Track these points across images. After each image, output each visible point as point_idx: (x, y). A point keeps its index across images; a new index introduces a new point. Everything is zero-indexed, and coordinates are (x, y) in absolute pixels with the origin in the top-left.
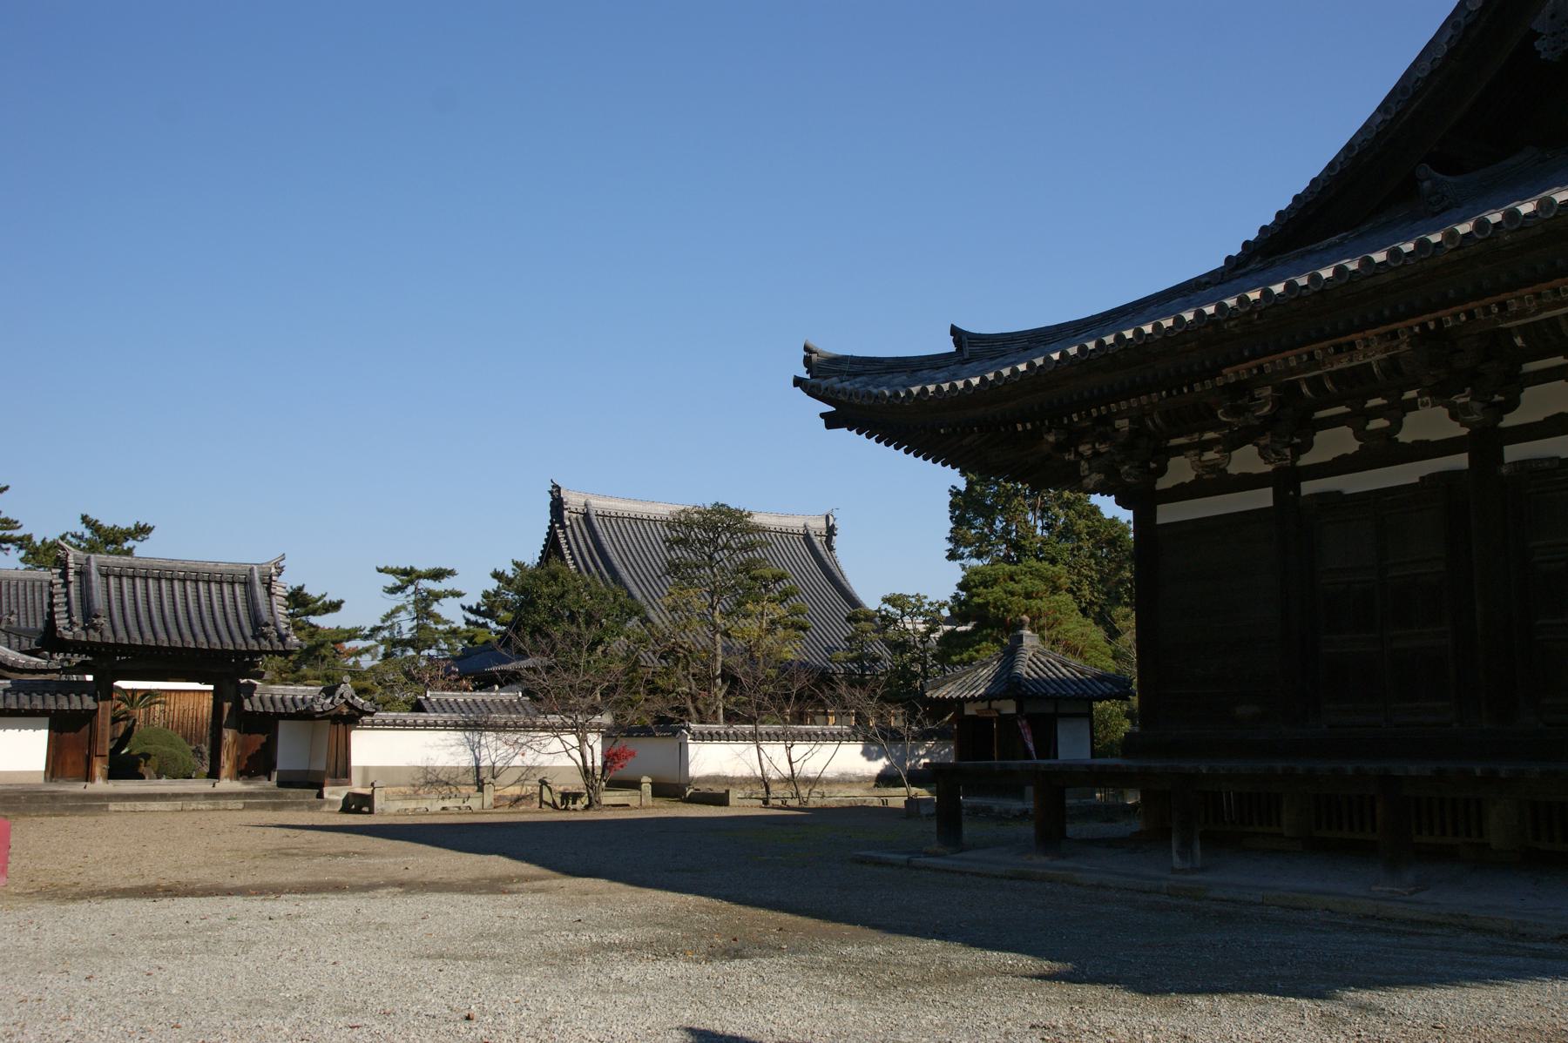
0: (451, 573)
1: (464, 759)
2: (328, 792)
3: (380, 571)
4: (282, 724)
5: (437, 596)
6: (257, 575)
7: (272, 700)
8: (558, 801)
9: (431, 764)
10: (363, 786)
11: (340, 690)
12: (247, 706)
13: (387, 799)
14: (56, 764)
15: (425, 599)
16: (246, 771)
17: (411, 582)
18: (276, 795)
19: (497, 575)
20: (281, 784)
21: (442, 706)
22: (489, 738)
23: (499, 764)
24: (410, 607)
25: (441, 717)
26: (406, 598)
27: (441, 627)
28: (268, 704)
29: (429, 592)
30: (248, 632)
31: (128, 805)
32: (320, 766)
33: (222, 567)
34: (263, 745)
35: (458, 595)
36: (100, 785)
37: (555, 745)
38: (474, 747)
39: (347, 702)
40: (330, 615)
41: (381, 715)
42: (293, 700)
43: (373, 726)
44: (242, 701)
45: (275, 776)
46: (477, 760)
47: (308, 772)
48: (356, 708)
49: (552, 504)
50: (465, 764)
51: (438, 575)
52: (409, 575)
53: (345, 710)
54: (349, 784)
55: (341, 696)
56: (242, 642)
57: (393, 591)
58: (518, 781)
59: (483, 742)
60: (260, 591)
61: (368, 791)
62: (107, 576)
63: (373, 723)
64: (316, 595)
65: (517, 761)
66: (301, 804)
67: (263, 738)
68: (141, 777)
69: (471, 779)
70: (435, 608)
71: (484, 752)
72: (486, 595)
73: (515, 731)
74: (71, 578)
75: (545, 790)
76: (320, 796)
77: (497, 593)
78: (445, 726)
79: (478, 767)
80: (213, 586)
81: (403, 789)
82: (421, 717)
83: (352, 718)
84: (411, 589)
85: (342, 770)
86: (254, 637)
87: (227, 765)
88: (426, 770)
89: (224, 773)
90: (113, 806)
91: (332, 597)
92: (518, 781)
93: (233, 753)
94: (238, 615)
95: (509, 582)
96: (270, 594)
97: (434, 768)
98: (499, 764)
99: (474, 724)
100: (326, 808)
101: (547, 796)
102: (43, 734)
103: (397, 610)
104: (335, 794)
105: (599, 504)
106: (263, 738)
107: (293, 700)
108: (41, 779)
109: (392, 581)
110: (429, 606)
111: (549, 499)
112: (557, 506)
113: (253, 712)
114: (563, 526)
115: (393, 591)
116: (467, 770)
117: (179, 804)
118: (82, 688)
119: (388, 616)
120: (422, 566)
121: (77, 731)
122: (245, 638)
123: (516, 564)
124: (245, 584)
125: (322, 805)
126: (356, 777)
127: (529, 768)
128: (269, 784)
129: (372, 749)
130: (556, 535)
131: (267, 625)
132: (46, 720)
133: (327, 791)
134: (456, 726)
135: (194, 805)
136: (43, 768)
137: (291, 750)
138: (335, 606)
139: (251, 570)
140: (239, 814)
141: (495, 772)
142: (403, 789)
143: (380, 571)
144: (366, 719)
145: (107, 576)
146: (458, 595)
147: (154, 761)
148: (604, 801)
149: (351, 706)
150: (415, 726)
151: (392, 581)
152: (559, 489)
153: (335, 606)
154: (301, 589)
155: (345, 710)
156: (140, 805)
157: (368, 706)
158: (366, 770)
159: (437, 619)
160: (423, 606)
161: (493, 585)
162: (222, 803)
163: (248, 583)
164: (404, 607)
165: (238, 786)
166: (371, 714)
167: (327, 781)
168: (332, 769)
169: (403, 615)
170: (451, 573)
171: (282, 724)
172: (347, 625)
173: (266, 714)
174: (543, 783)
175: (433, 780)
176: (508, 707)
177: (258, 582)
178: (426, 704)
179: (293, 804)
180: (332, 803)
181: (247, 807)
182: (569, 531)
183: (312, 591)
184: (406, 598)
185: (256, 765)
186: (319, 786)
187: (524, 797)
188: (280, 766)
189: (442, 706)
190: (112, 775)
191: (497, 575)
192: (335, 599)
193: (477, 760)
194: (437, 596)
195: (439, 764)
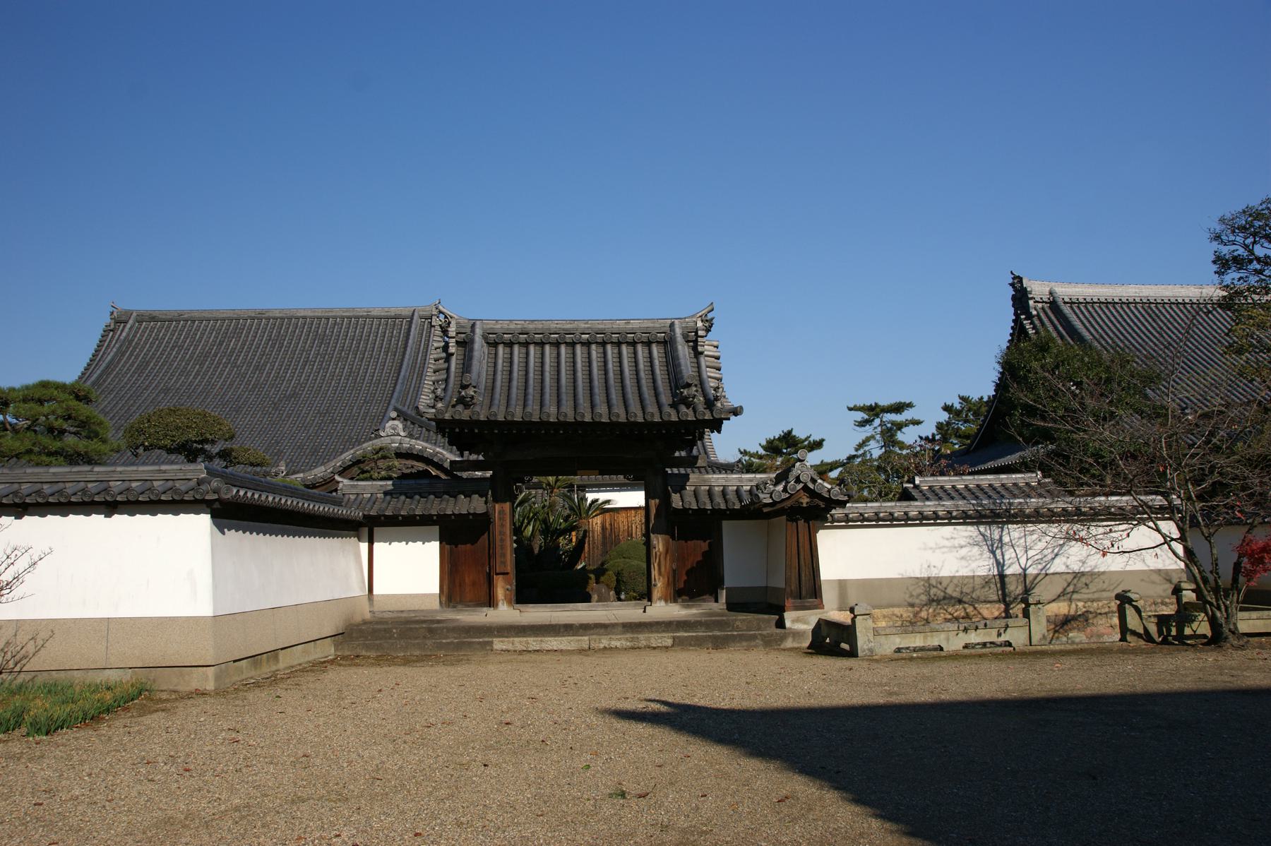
0: (910, 405)
1: (982, 566)
2: (791, 618)
3: (850, 409)
4: (726, 525)
5: (900, 426)
6: (678, 331)
7: (710, 493)
8: (1153, 629)
9: (934, 573)
10: (841, 609)
11: (795, 472)
12: (676, 501)
13: (876, 632)
14: (460, 581)
15: (890, 430)
16: (684, 591)
17: (877, 415)
18: (720, 625)
19: (947, 408)
20: (732, 606)
21: (936, 494)
22: (1014, 532)
23: (1032, 571)
24: (878, 437)
25: (930, 506)
26: (873, 429)
27: (904, 452)
28: (704, 498)
29: (893, 423)
30: (666, 398)
31: (519, 643)
32: (779, 582)
33: (635, 325)
34: (704, 554)
35: (917, 423)
36: (504, 612)
37: (1143, 535)
38: (994, 547)
39: (805, 488)
40: (815, 452)
41: (853, 508)
42: (738, 492)
43: (848, 523)
44: (670, 496)
45: (723, 595)
46: (1000, 565)
47: (766, 589)
48: (820, 496)
49: (1014, 298)
50: (982, 572)
51: (899, 408)
52: (874, 411)
53: (805, 500)
54: (820, 606)
55: (798, 480)
56: (656, 409)
57: (862, 424)
58: (1062, 595)
59: (1006, 539)
60: (683, 351)
61: (843, 617)
62: (494, 345)
63: (847, 519)
64: (803, 437)
65: (1058, 566)
66: (754, 637)
67: (704, 546)
68: (587, 599)
69: (993, 594)
70: (900, 436)
71: (1009, 554)
72: (940, 426)
73: (1050, 522)
74: (452, 350)
75: (1130, 612)
76: (781, 624)
77: (948, 423)
78: (950, 519)
79: (1002, 576)
80: (624, 347)
81: (897, 611)
82: (914, 508)
83: (816, 511)
84: (877, 422)
85: (808, 587)
86: (674, 406)
87: (659, 585)
88: (928, 582)
89: (656, 593)
90: (499, 644)
91: (816, 437)
92: (1062, 595)
93: (667, 565)
94: (654, 381)
95: (957, 413)
96: (698, 354)
97: (939, 580)
98: (1032, 571)
99: (990, 515)
100: (789, 643)
101: (1133, 621)
102: (434, 548)
103: (867, 440)
104: (801, 622)
105: (1066, 291)
106: (704, 546)
107: (738, 492)
108: (435, 605)
109: (860, 416)
110: (893, 435)
111: (1011, 292)
112: (1021, 297)
113: (685, 510)
114: (1029, 317)
115: (862, 424)
116: (987, 581)
117: (584, 641)
118: (474, 488)
119: (860, 446)
120: (884, 402)
121: (474, 542)
122: (660, 406)
123: (962, 398)
124: (664, 343)
125: (783, 638)
126: (829, 596)
127: (1077, 575)
128: (716, 607)
129: (850, 556)
130: (1022, 324)
131: (688, 386)
132: (437, 528)
133: (789, 617)
134: (965, 519)
135: (605, 642)
136: (437, 590)
137: (741, 560)
138: (818, 445)
139: (672, 325)
140: (663, 657)
141: (1028, 584)
142: (897, 611)
143: (850, 409)
144: (838, 512)
145: (494, 345)
146: (917, 423)
147: (610, 576)
148: (1243, 627)
149: (812, 494)
150: (906, 521)
151: (860, 416)
152: (1020, 279)
153: (818, 445)
154: (790, 432)
155: (805, 500)
156: (533, 643)
157: (837, 493)
158: (842, 585)
159: (902, 445)
160: (889, 435)
161: (944, 417)
162: (643, 638)
163: (668, 343)
164: (873, 437)
165: (675, 611)
166: (842, 504)
167: (789, 603)
168: (794, 586)
169: (872, 444)
170: (910, 405)
171: (726, 525)
172: (829, 460)
173: (701, 512)
174: (1124, 599)
175: (937, 599)
176: (1027, 491)
177: (679, 338)
178: (915, 493)
179: (741, 638)
180: (797, 635)
181: (679, 643)
182: (1037, 322)
183: (800, 433)
184: (873, 429)
185: (697, 582)
186: (779, 610)
187: (1074, 618)
188: (728, 582)
189: (936, 494)
190: (523, 596)
191: (947, 408)
192: (818, 439)
193: (1000, 565)
194: (900, 426)
195: (946, 572)
